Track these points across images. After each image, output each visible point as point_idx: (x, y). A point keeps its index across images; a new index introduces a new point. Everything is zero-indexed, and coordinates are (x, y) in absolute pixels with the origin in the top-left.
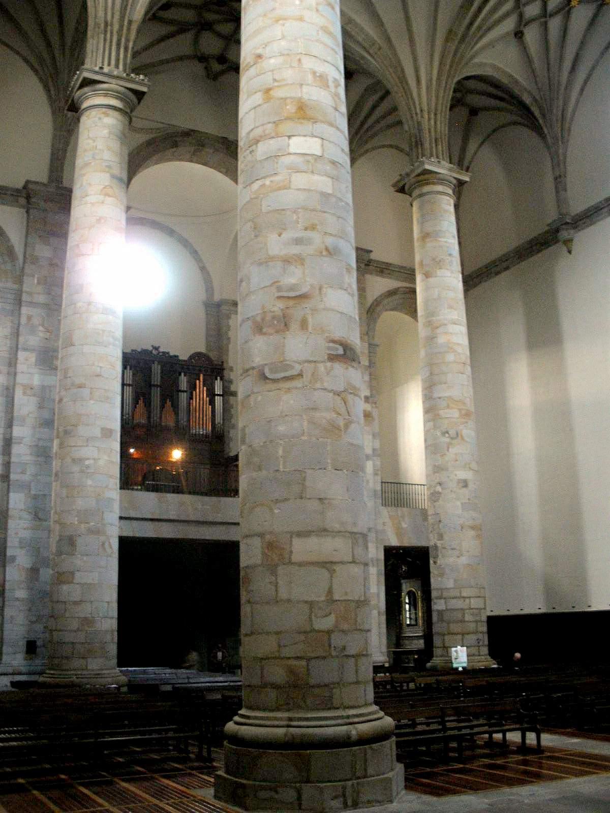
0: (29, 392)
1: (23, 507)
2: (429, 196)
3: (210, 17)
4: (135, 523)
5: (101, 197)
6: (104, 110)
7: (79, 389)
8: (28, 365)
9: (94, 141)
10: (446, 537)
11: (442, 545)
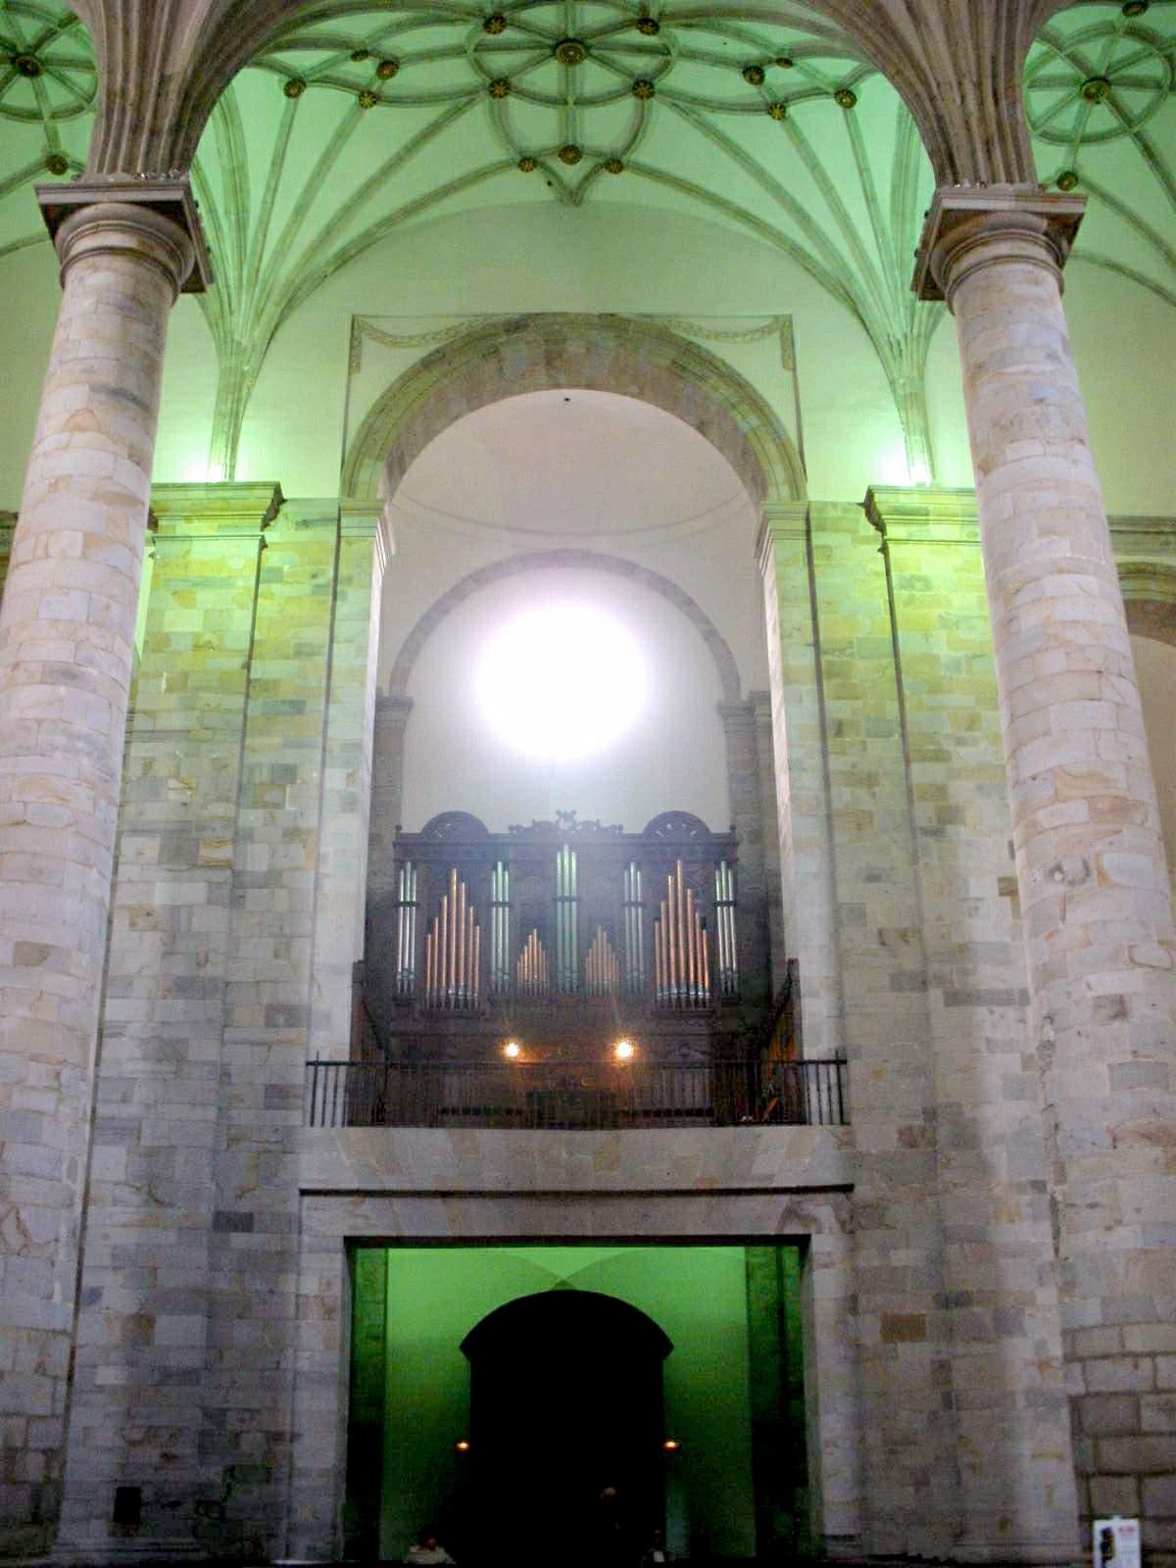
0: (141, 922)
1: (122, 1177)
2: (981, 274)
3: (499, 62)
4: (398, 1204)
5: (64, 437)
6: (91, 260)
8: (142, 865)
10: (1074, 1174)
11: (1064, 1194)
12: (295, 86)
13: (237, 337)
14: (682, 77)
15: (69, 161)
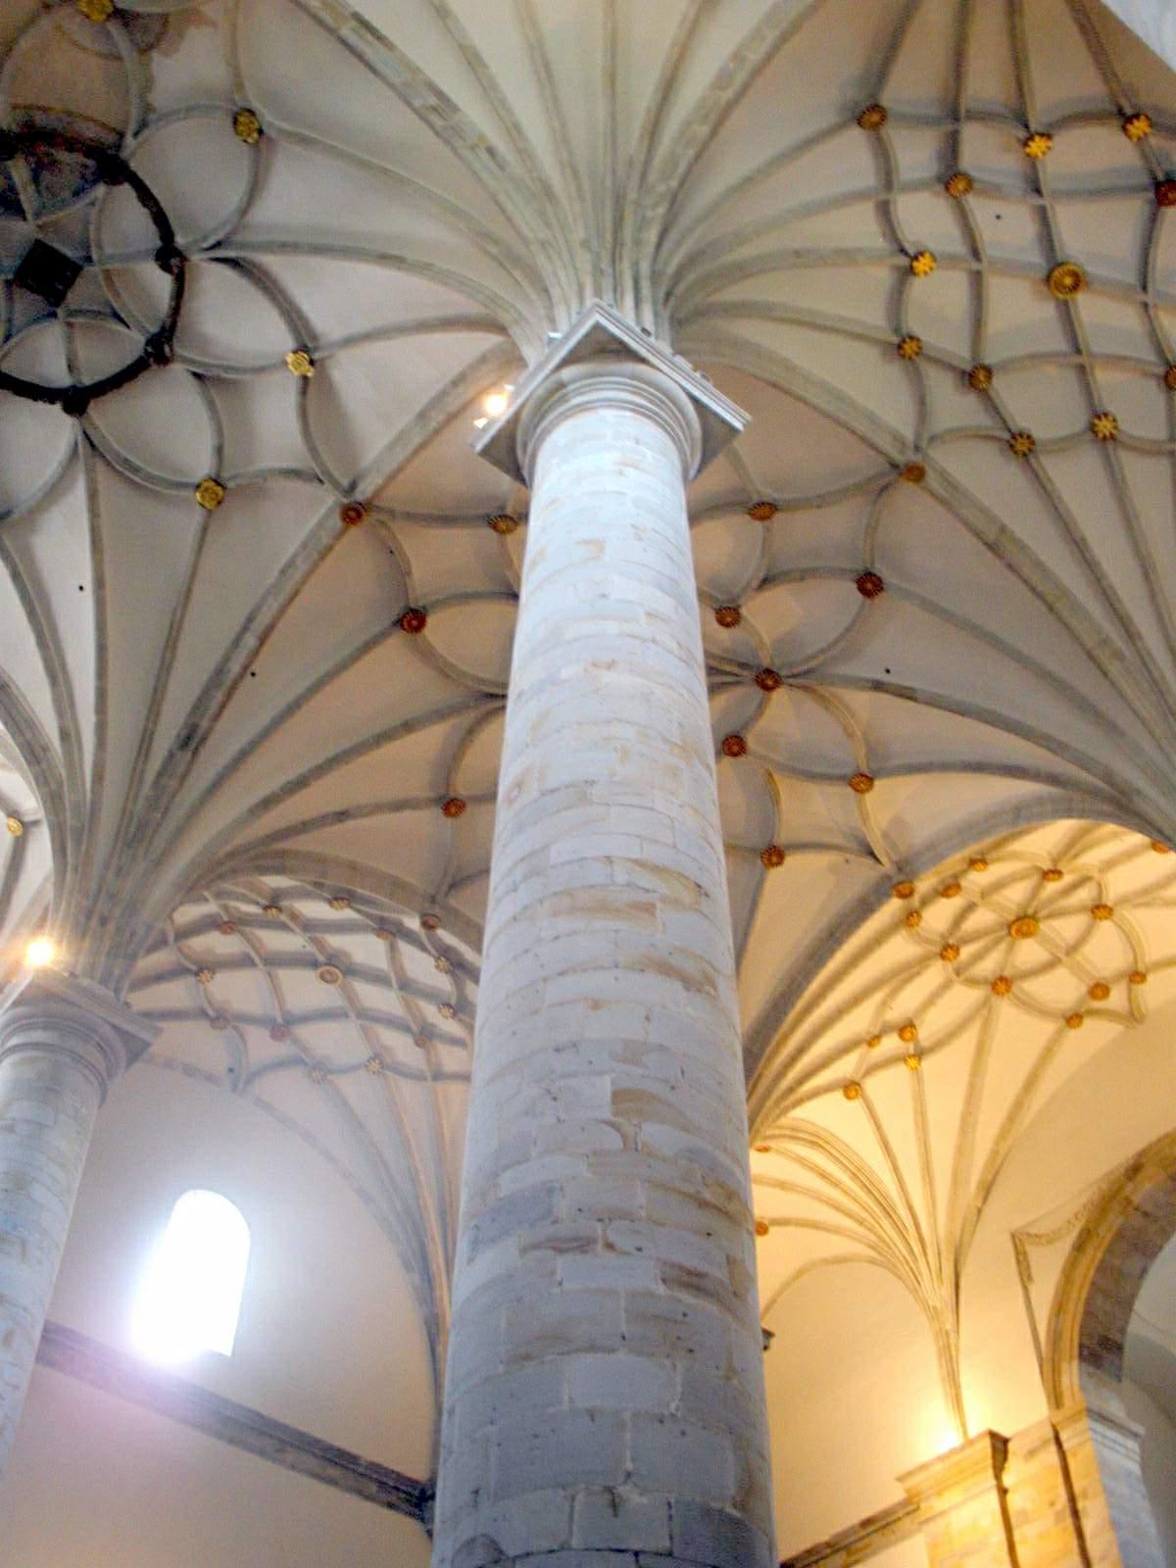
12: (851, 1088)
13: (931, 1303)
15: (766, 1222)
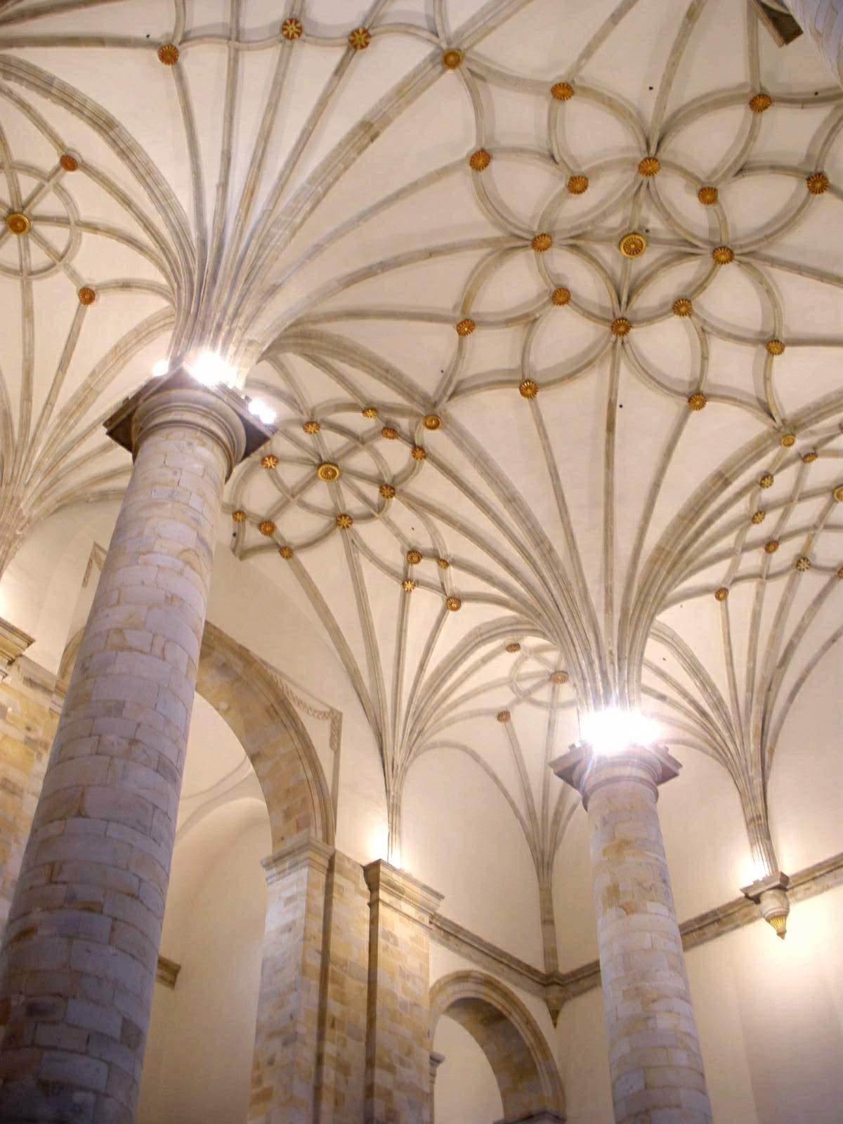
7: (86, 914)
9: (175, 473)
14: (370, 532)
